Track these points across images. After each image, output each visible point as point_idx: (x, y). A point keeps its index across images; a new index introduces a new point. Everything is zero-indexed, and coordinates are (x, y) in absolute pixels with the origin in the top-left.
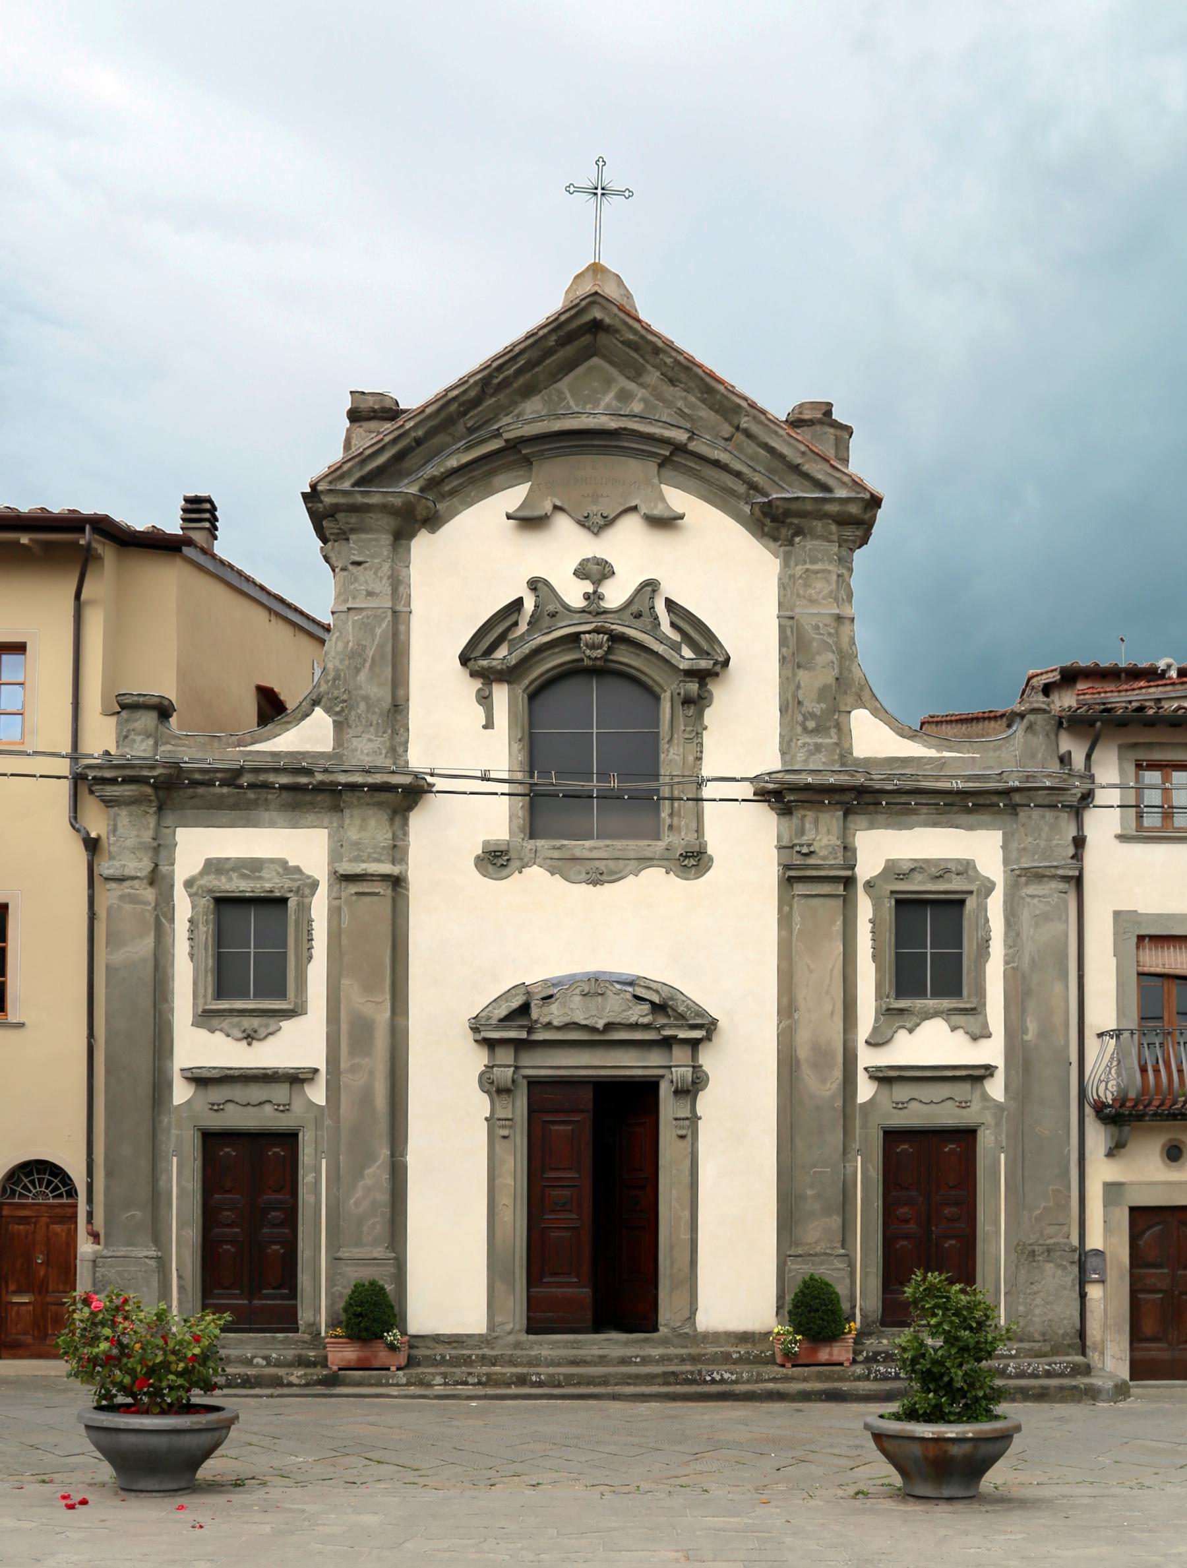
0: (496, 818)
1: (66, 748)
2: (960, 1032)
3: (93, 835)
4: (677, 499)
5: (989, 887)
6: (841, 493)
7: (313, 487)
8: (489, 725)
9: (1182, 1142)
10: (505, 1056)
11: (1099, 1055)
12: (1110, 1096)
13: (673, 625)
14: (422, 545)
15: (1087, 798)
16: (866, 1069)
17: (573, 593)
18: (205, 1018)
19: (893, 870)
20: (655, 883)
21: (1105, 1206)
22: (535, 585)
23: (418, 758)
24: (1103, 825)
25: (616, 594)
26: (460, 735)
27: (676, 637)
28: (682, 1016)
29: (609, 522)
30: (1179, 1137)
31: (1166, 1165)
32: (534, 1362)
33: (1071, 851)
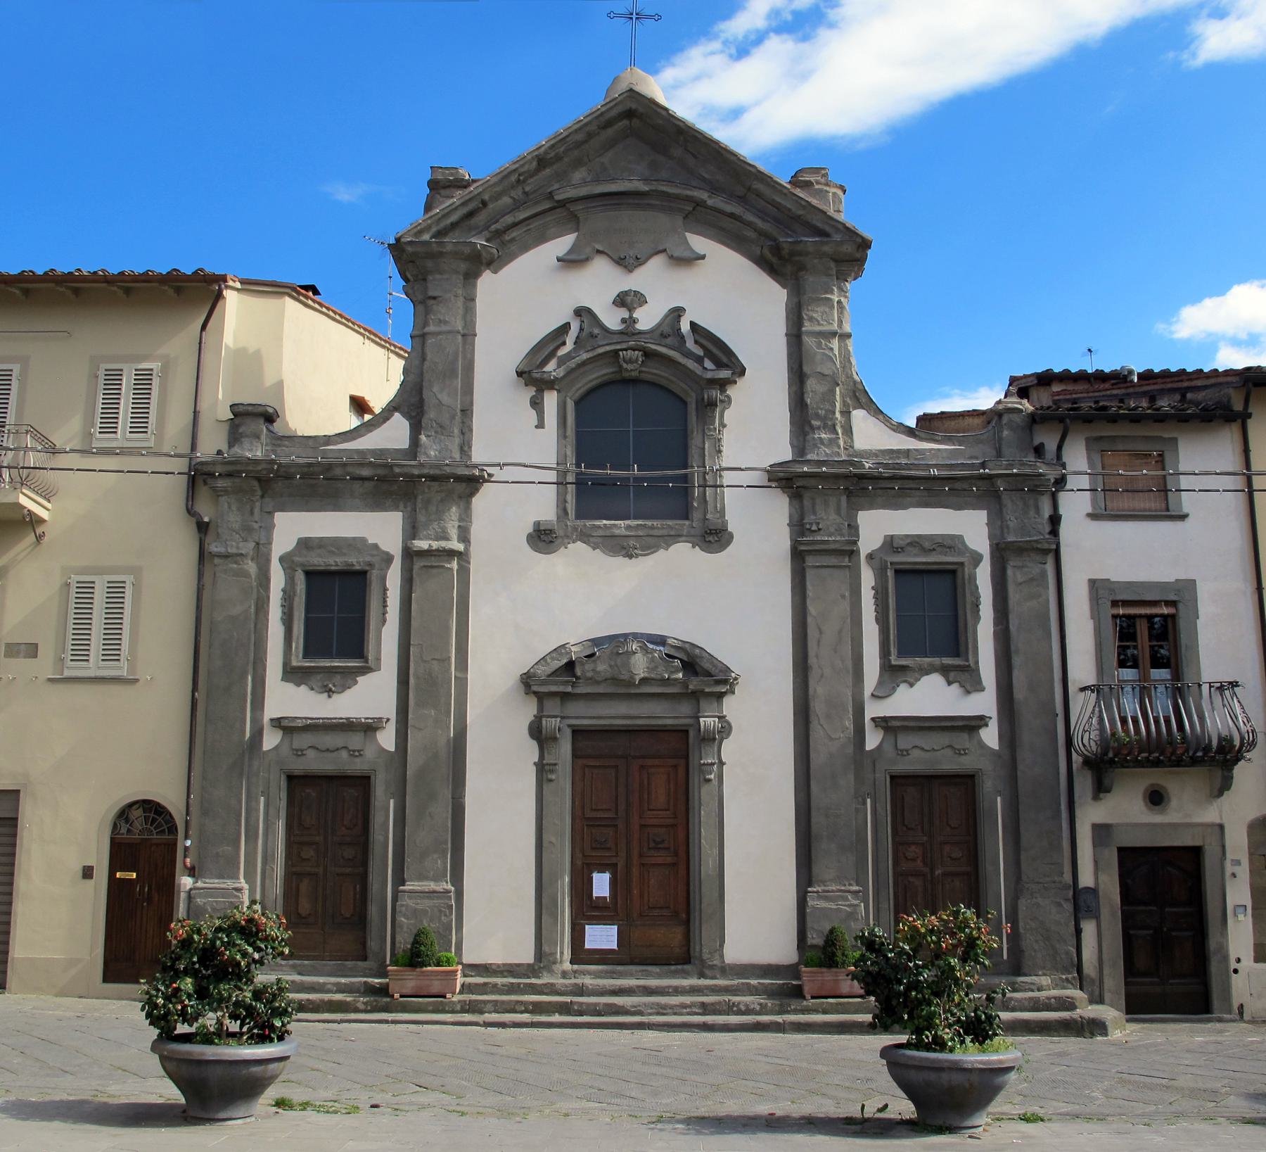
0: (542, 504)
1: (186, 449)
2: (955, 685)
3: (206, 519)
4: (698, 243)
5: (977, 558)
6: (837, 237)
7: (398, 240)
8: (540, 425)
9: (1164, 788)
10: (552, 706)
11: (1082, 706)
12: (1094, 748)
13: (696, 342)
14: (487, 283)
15: (1061, 482)
16: (873, 719)
17: (612, 319)
18: (292, 674)
19: (891, 544)
20: (683, 554)
21: (1094, 846)
22: (581, 312)
23: (479, 454)
24: (1075, 505)
25: (647, 318)
26: (518, 443)
27: (700, 352)
28: (709, 674)
29: (639, 262)
30: (1162, 782)
31: (1150, 809)
32: (580, 991)
33: (1048, 529)
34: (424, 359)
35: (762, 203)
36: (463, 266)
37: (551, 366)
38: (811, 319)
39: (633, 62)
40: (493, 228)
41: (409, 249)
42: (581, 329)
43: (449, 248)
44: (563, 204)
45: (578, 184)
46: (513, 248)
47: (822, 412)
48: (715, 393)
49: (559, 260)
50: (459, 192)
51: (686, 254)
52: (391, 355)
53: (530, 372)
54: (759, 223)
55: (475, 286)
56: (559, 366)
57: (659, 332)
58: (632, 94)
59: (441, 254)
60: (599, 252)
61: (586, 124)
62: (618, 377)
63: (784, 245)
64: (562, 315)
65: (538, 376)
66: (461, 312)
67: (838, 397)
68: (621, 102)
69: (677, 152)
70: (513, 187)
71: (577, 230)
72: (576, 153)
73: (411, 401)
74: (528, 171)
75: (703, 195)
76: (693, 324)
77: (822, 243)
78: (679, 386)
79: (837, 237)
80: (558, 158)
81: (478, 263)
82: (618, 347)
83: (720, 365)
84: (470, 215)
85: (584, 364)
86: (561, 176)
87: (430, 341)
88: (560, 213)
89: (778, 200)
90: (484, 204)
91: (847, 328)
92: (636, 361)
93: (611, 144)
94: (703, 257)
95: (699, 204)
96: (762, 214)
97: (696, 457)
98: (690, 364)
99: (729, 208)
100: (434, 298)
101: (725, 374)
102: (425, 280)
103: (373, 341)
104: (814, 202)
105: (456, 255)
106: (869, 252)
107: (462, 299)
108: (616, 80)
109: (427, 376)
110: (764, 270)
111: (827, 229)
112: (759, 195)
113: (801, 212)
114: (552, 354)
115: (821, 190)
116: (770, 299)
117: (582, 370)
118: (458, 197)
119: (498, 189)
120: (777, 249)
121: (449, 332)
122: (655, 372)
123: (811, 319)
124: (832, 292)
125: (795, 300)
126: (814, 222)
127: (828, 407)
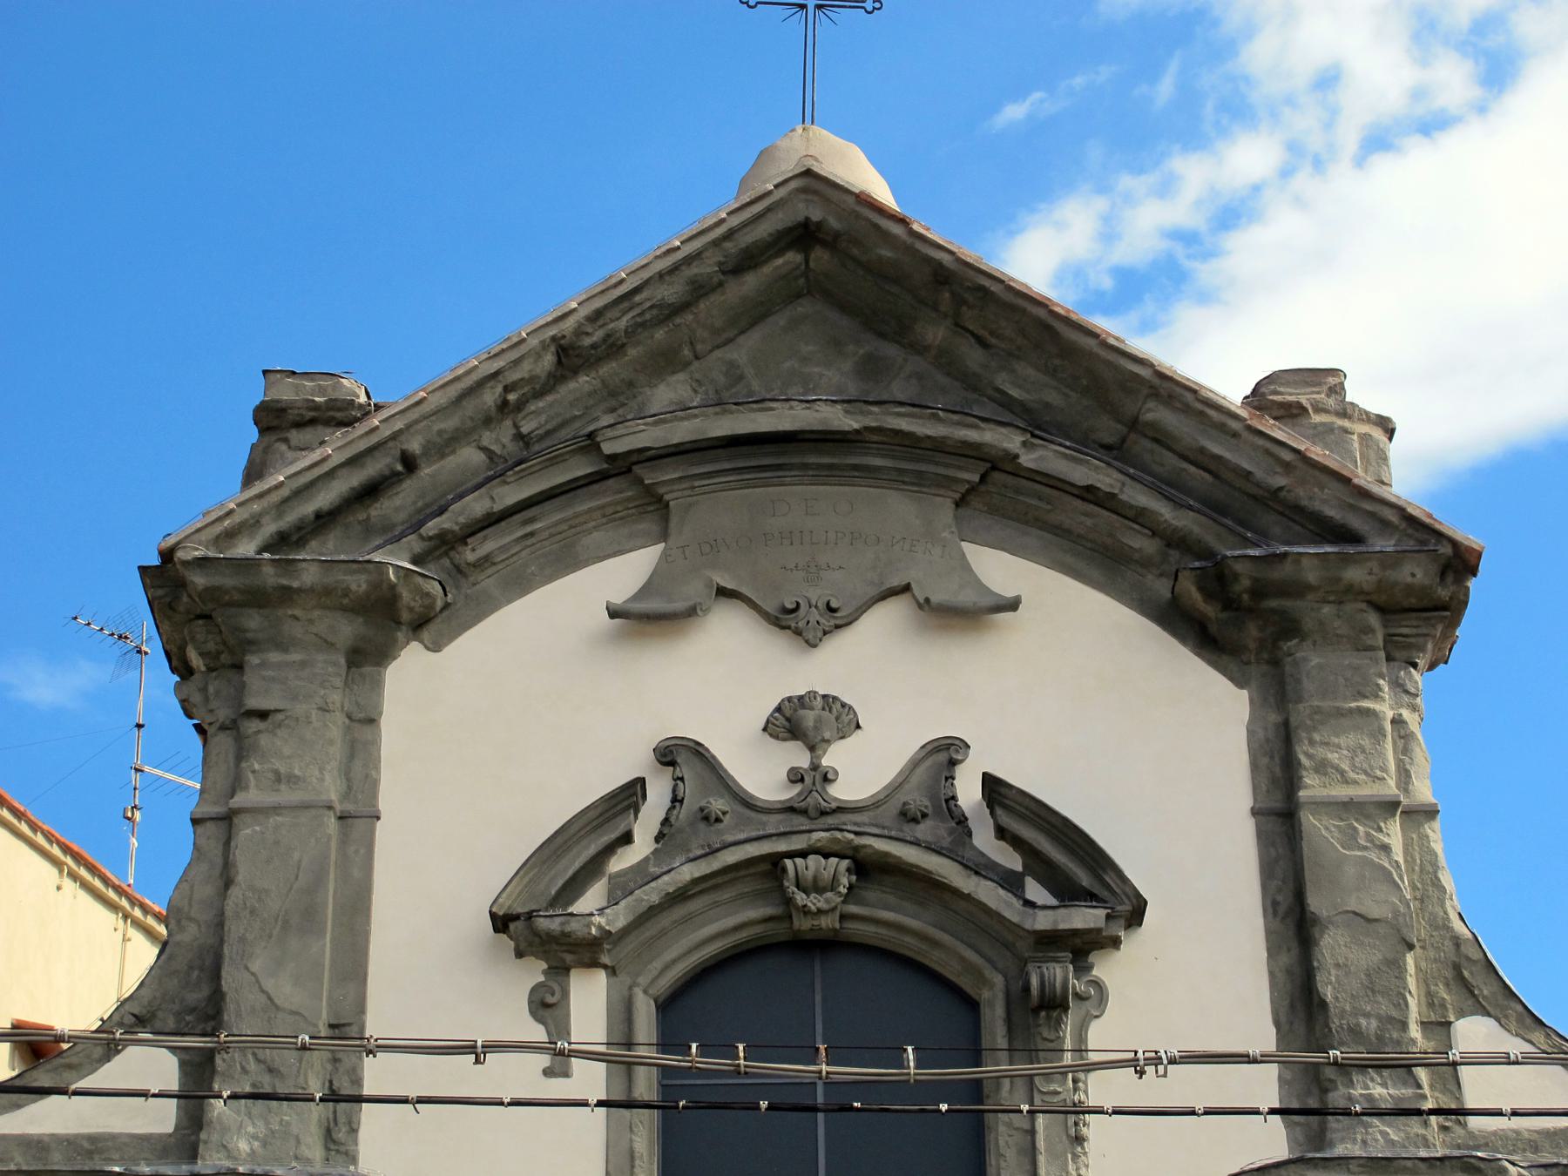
4: (997, 568)
6: (1384, 544)
7: (167, 555)
13: (1001, 833)
14: (411, 673)
17: (762, 772)
25: (862, 770)
27: (1012, 860)
29: (837, 619)
34: (228, 883)
35: (1171, 460)
36: (346, 629)
37: (591, 900)
38: (1322, 767)
39: (807, 115)
40: (432, 527)
41: (199, 580)
42: (676, 800)
43: (309, 576)
44: (623, 466)
45: (669, 413)
46: (488, 582)
47: (1370, 1025)
48: (1059, 972)
49: (614, 613)
50: (338, 436)
51: (966, 598)
52: (133, 933)
53: (530, 916)
54: (1165, 512)
55: (377, 685)
56: (613, 901)
57: (893, 808)
58: (812, 181)
59: (286, 595)
60: (723, 593)
61: (689, 260)
62: (780, 931)
63: (1239, 567)
64: (626, 759)
65: (554, 925)
66: (337, 751)
67: (1412, 983)
68: (780, 203)
69: (935, 333)
70: (488, 422)
71: (664, 536)
72: (660, 334)
73: (188, 1002)
74: (532, 379)
75: (1010, 441)
76: (993, 787)
77: (1345, 559)
78: (953, 955)
79: (1384, 544)
80: (613, 347)
81: (386, 621)
82: (782, 846)
83: (1068, 893)
84: (371, 492)
85: (680, 896)
86: (617, 396)
87: (246, 832)
88: (614, 492)
89: (1216, 449)
90: (410, 463)
91: (1424, 791)
92: (833, 885)
93: (754, 314)
94: (1013, 605)
95: (997, 464)
96: (1170, 487)
97: (1011, 1154)
98: (988, 893)
99: (1081, 474)
100: (263, 715)
101: (1085, 918)
102: (239, 667)
103: (85, 886)
104: (1317, 452)
105: (329, 598)
106: (1473, 584)
107: (340, 718)
108: (765, 156)
109: (234, 929)
110: (1183, 639)
111: (1356, 523)
112: (1161, 438)
113: (1280, 481)
114: (593, 868)
115: (1329, 428)
116: (1210, 714)
117: (679, 912)
118: (333, 446)
119: (450, 424)
120: (1217, 579)
121: (306, 806)
122: (887, 916)
123: (1322, 767)
124: (1376, 695)
125: (1274, 717)
126: (1317, 506)
127: (1385, 1008)
